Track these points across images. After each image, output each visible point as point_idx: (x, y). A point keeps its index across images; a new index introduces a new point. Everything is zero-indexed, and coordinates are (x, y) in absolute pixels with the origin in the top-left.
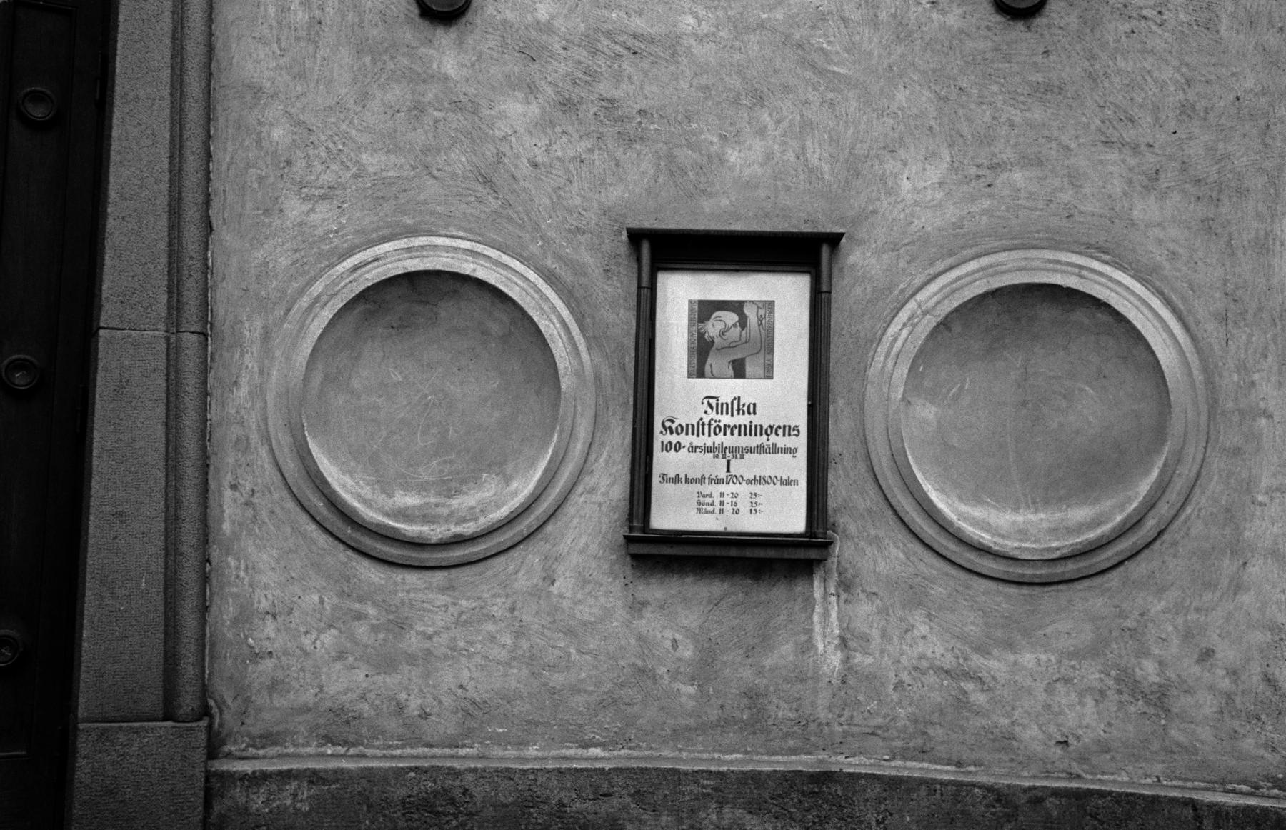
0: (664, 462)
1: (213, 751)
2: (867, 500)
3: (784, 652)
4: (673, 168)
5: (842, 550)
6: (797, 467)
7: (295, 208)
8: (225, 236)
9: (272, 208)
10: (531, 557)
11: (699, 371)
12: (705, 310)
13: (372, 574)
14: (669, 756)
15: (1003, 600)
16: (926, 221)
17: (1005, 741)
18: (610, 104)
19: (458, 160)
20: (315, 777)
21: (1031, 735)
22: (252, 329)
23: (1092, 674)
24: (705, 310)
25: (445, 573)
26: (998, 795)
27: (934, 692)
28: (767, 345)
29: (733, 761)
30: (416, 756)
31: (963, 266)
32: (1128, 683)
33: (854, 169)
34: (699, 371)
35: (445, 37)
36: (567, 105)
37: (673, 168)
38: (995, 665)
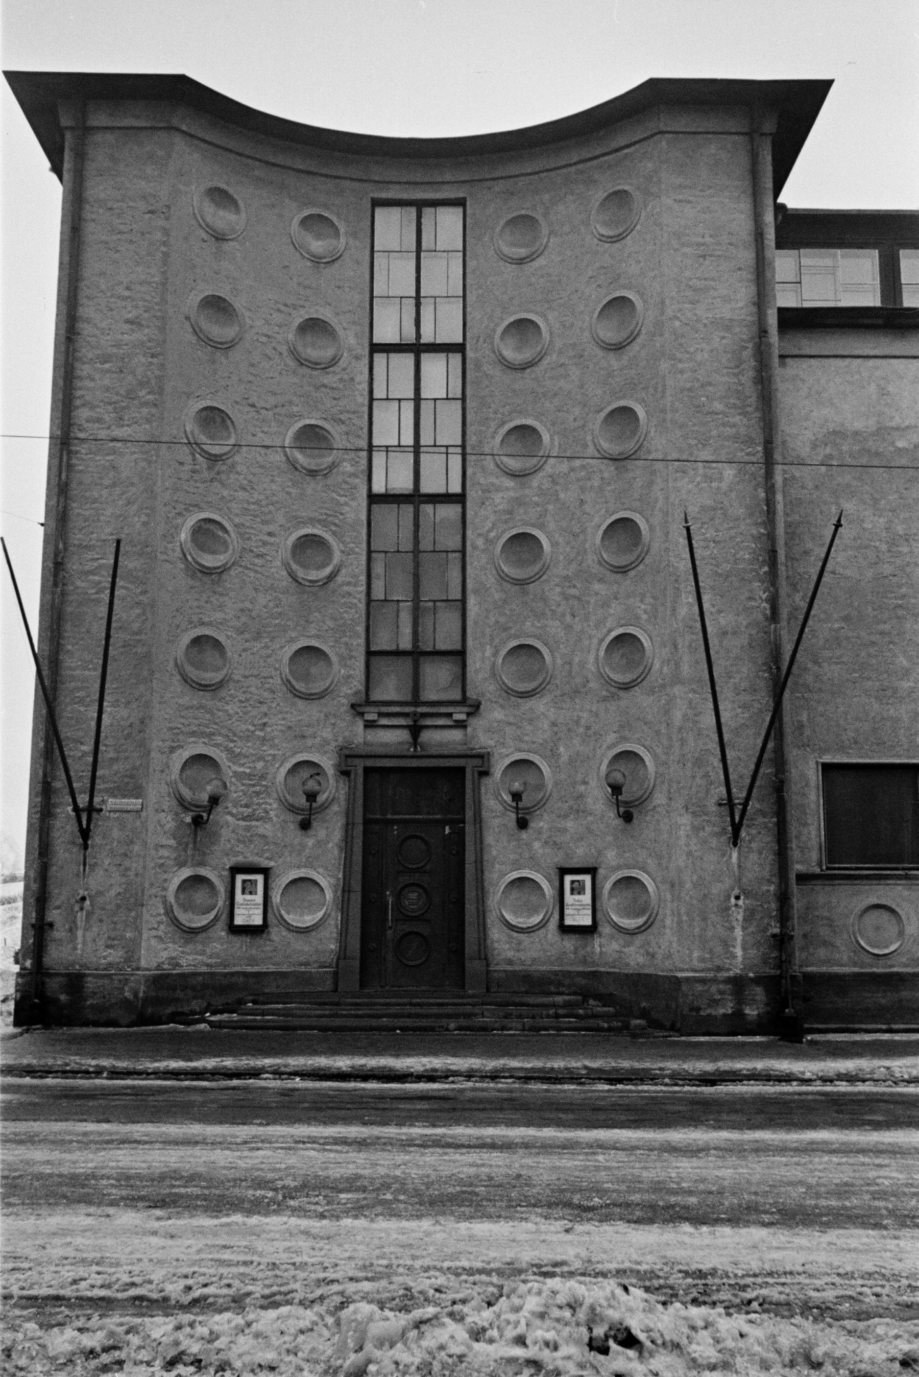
0: (567, 912)
1: (488, 965)
2: (275, 921)
3: (589, 949)
4: (567, 855)
5: (600, 929)
6: (590, 912)
7: (497, 866)
8: (486, 873)
9: (493, 867)
10: (543, 931)
11: (572, 893)
12: (573, 882)
13: (515, 934)
14: (569, 968)
15: (627, 937)
16: (614, 863)
17: (628, 965)
18: (555, 842)
19: (527, 855)
20: (505, 971)
21: (632, 963)
22: (491, 890)
23: (642, 951)
24: (573, 882)
25: (106, 615)
26: (627, 975)
27: (615, 955)
28: (584, 889)
29: (581, 969)
30: (524, 968)
31: (793, 798)
32: (648, 953)
33: (600, 853)
34: (572, 893)
35: (523, 832)
36: (546, 843)
37: (567, 855)
38: (626, 950)
